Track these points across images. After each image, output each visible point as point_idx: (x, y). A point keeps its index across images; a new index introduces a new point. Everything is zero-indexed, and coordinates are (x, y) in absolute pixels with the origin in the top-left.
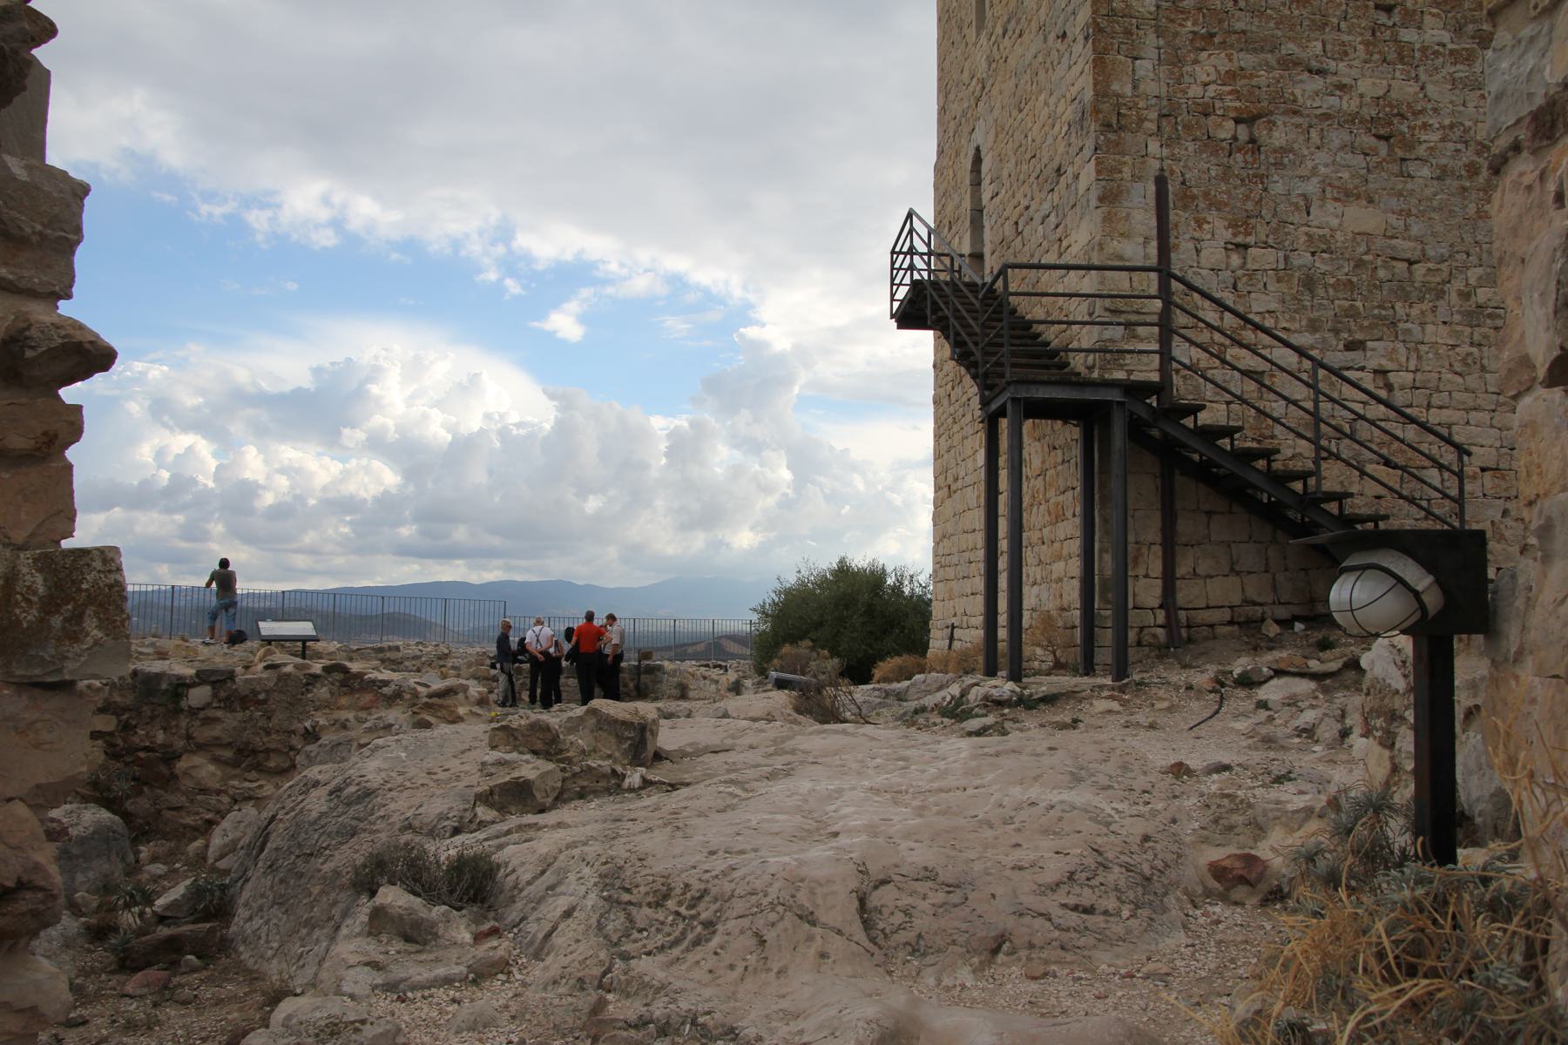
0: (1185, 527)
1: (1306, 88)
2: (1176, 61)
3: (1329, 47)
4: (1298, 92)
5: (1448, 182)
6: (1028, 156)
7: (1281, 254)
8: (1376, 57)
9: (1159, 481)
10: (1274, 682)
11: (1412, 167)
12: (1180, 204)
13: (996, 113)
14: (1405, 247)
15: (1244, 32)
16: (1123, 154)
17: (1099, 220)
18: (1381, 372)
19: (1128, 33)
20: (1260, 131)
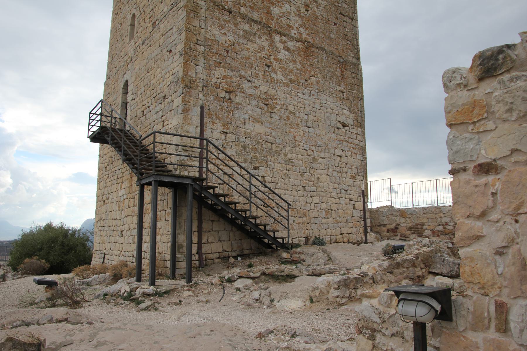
0: (205, 226)
1: (246, 85)
2: (210, 69)
3: (253, 74)
4: (244, 86)
5: (282, 121)
6: (151, 89)
7: (237, 137)
8: (265, 80)
9: (197, 210)
10: (239, 280)
11: (273, 115)
12: (207, 116)
13: (136, 70)
14: (271, 139)
15: (229, 64)
16: (191, 97)
17: (182, 118)
18: (263, 177)
19: (195, 56)
20: (232, 96)
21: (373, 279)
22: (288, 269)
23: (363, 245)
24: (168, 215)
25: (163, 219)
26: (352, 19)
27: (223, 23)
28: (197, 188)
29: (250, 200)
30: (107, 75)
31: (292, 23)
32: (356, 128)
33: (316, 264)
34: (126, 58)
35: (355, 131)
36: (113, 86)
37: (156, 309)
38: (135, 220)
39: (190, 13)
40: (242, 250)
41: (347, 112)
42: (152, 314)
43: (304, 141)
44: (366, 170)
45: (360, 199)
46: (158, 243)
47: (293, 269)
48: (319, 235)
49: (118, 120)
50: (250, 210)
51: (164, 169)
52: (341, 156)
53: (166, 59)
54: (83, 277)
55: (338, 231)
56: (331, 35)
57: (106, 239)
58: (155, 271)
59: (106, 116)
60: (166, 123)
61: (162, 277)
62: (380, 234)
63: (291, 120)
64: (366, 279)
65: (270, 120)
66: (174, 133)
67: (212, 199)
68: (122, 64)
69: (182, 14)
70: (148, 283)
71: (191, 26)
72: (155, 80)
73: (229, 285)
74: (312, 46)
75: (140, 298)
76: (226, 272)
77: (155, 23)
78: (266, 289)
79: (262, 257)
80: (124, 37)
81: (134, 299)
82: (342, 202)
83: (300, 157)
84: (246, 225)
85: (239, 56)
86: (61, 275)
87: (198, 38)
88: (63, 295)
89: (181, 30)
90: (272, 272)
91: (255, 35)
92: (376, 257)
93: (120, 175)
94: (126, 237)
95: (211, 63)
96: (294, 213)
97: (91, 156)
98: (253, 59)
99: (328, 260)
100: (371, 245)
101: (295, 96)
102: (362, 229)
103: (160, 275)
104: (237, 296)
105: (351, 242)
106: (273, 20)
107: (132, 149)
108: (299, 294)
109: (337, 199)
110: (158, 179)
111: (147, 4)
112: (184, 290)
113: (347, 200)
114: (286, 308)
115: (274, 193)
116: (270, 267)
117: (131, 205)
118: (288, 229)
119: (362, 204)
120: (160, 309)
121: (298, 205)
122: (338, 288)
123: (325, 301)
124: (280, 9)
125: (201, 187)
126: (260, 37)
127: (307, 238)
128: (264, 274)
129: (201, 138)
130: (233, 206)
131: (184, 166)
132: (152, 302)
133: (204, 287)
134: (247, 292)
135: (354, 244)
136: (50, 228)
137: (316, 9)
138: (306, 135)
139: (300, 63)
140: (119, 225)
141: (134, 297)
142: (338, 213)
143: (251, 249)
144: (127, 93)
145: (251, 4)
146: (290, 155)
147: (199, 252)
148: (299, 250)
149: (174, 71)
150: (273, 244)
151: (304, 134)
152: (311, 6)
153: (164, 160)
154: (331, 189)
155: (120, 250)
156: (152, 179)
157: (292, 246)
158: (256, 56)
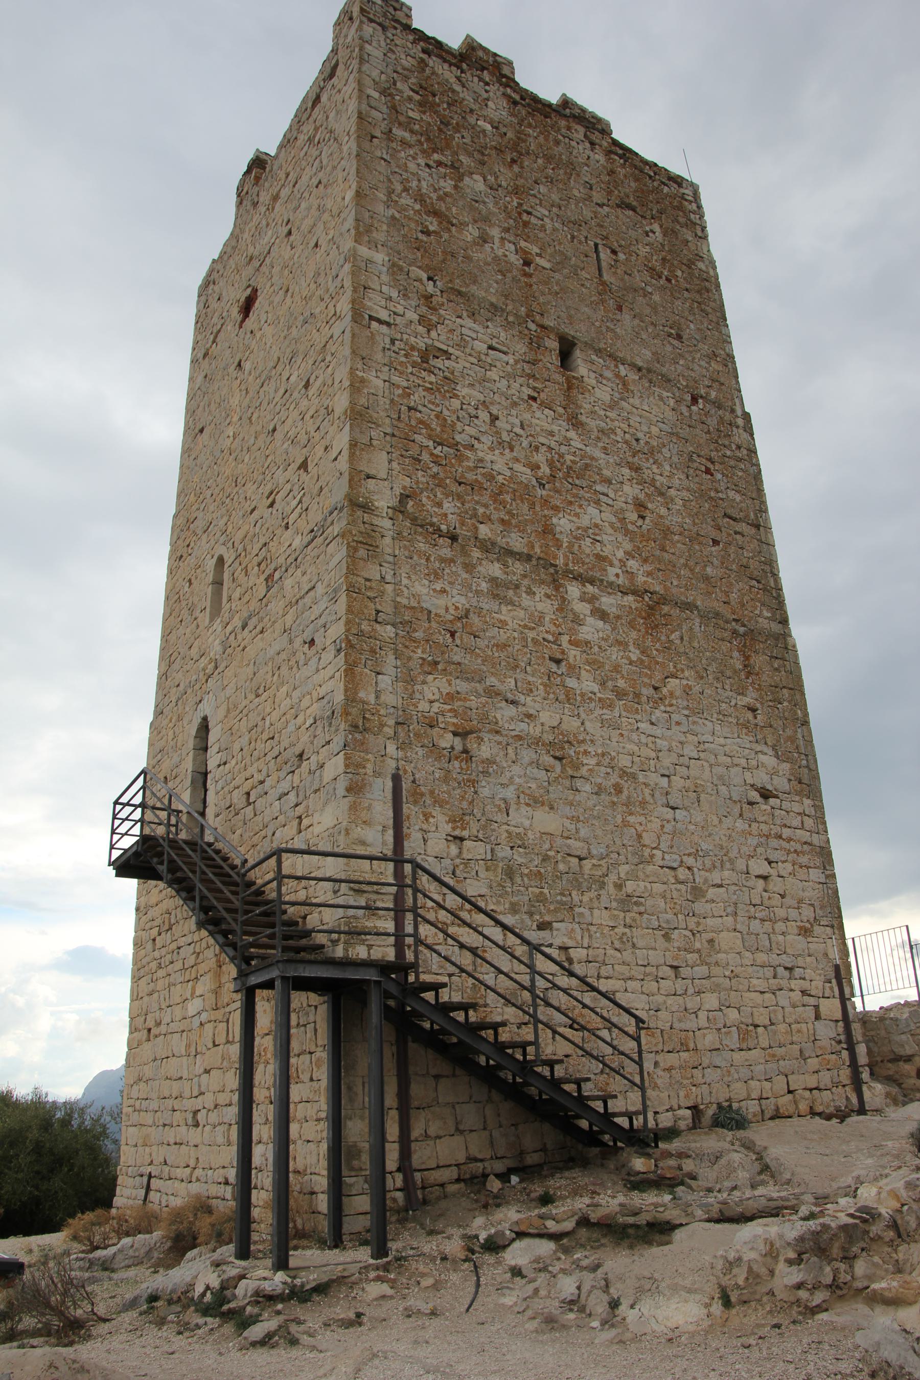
1: (504, 714)
3: (519, 684)
4: (499, 716)
5: (603, 797)
6: (265, 736)
7: (488, 847)
8: (551, 696)
9: (394, 1048)
10: (517, 1244)
11: (579, 783)
13: (229, 691)
14: (577, 846)
15: (459, 664)
17: (346, 807)
18: (564, 949)
19: (373, 651)
20: (472, 744)
21: (894, 1225)
22: (653, 1203)
23: (855, 1118)
24: (318, 1067)
25: (305, 1077)
26: (758, 527)
27: (437, 565)
28: (393, 989)
29: (534, 1016)
30: (156, 706)
31: (607, 551)
32: (797, 798)
33: (728, 1184)
34: (203, 662)
35: (797, 808)
36: (171, 733)
37: (294, 1342)
38: (233, 1081)
39: (356, 550)
40: (522, 1153)
41: (769, 760)
42: (279, 1357)
43: (663, 846)
44: (839, 909)
45: (831, 988)
46: (294, 1142)
47: (664, 1205)
48: (729, 1100)
49: (184, 818)
50: (535, 1043)
51: (304, 942)
52: (765, 878)
53: (301, 663)
54: (92, 1243)
55: (780, 1084)
56: (709, 570)
57: (155, 1134)
58: (287, 1224)
59: (154, 808)
60: (305, 822)
61: (305, 1242)
62: (900, 1085)
63: (626, 792)
64: (875, 1229)
65: (571, 798)
66: (328, 849)
67: (434, 1018)
68: (194, 677)
69: (338, 553)
70: (269, 1262)
71: (359, 579)
72: (275, 715)
73: (489, 1258)
74: (663, 600)
75: (249, 1308)
76: (479, 1221)
77: (271, 576)
78: (595, 1268)
79: (576, 1173)
80: (197, 613)
81: (231, 1312)
82: (783, 1002)
83: (658, 888)
84: (526, 1084)
85: (481, 643)
86: (33, 1239)
87: (379, 608)
88: (37, 1300)
89: (335, 591)
90: (607, 1216)
91: (517, 587)
92: (897, 1157)
93: (191, 960)
94: (208, 1128)
95: (414, 664)
96: (654, 1041)
97: (115, 912)
98: (517, 647)
99: (760, 1173)
100: (878, 1118)
101: (632, 731)
102: (845, 1075)
103: (302, 1235)
104: (515, 1293)
105: (819, 1114)
106: (559, 547)
107: (222, 892)
108: (687, 1283)
109: (767, 995)
110: (291, 973)
111: (251, 533)
112: (368, 1280)
113: (796, 996)
114: (655, 1327)
115: (594, 989)
116: (602, 1199)
117: (220, 1039)
118: (642, 1088)
119: (837, 1002)
120: (305, 1339)
121: (663, 1020)
122: (798, 1261)
123: (765, 1299)
124: (574, 519)
125: (404, 986)
126: (530, 592)
127: (694, 1108)
128: (584, 1221)
129: (398, 858)
130: (489, 1034)
131: (356, 934)
132: (282, 1318)
133: (421, 1268)
134: (542, 1278)
135: (828, 1118)
136: (7, 1105)
137: (663, 511)
138: (668, 828)
139: (638, 646)
140: (187, 1094)
141: (232, 1305)
142: (775, 1033)
143: (544, 1149)
144: (206, 749)
145: (502, 515)
146: (630, 886)
147: (405, 1166)
148: (675, 1145)
149: (322, 691)
150: (602, 1132)
151: (662, 826)
152: (650, 506)
153: (305, 917)
154: (750, 969)
155: (192, 1163)
156: (274, 973)
157: (656, 1135)
158: (525, 639)
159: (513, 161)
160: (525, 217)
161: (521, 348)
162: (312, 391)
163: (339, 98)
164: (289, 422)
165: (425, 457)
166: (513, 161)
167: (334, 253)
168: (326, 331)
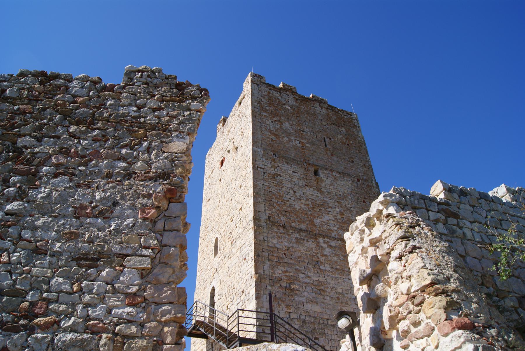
6: (232, 288)
11: (325, 297)
13: (220, 277)
31: (332, 228)
36: (202, 294)
149: (248, 272)
159: (297, 116)
160: (302, 132)
161: (302, 170)
162: (242, 188)
163: (246, 105)
164: (236, 197)
165: (275, 205)
166: (297, 116)
167: (247, 149)
168: (245, 171)
